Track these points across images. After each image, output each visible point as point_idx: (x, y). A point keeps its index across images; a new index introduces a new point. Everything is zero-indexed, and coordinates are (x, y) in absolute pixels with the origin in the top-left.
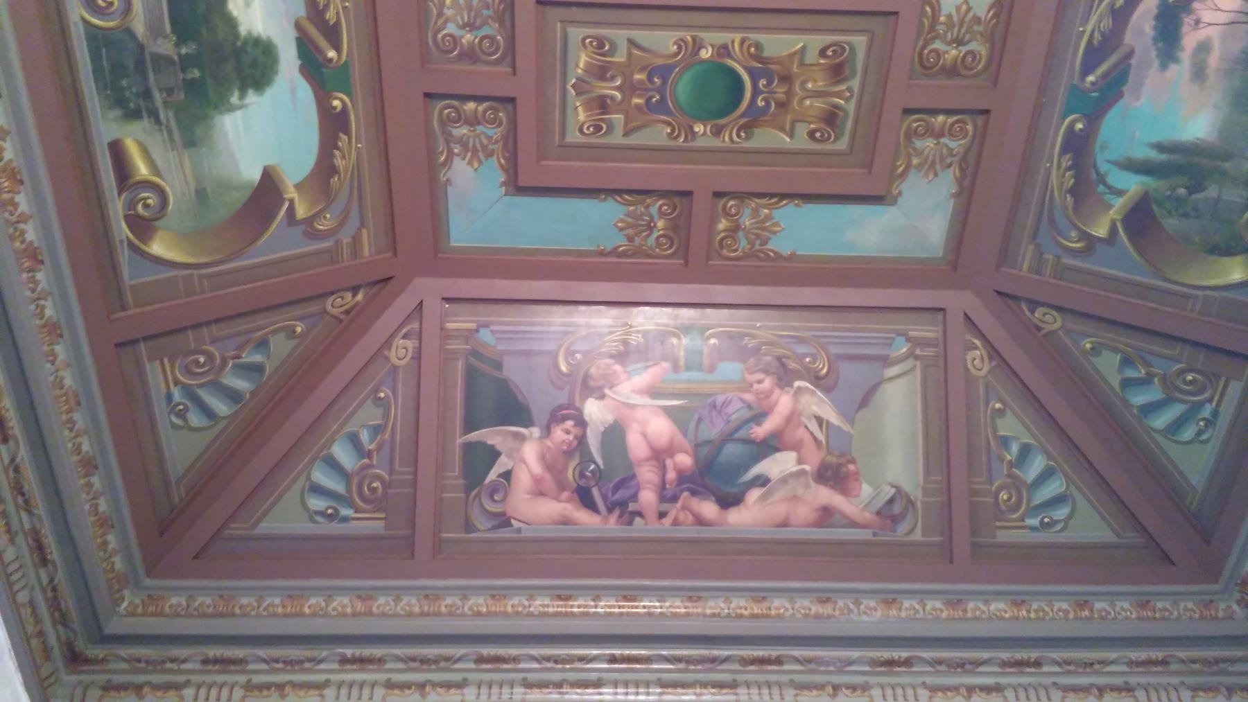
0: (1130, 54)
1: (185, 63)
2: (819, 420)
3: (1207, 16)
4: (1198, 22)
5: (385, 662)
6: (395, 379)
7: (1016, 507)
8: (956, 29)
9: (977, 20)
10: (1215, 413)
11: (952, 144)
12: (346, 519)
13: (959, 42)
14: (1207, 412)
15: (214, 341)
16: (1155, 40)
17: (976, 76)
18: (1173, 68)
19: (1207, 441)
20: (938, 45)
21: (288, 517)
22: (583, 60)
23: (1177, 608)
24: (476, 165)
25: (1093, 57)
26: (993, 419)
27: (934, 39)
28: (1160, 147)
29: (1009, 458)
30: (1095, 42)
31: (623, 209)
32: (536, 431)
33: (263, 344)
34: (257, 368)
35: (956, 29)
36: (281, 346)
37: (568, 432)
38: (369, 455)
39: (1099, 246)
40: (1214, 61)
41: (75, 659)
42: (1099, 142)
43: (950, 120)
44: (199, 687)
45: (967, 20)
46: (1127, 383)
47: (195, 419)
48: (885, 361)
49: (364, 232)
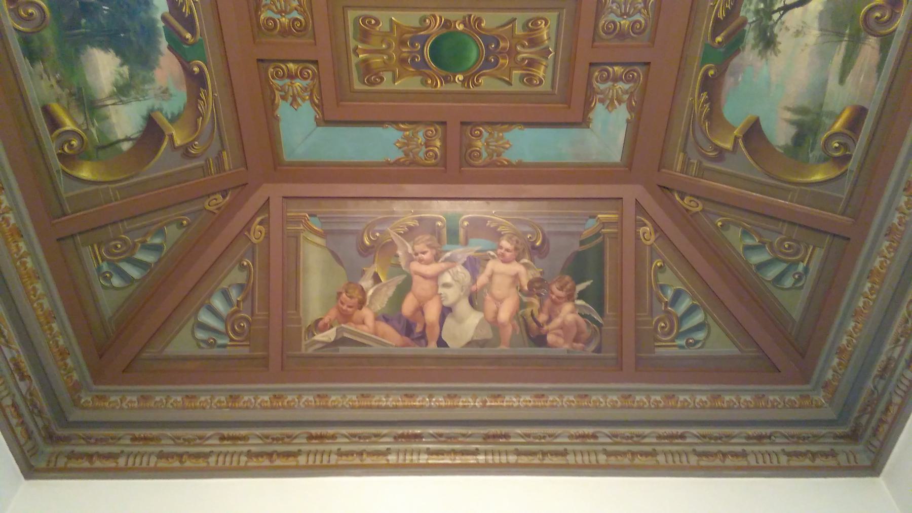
5: (248, 439)
6: (253, 252)
7: (669, 333)
10: (806, 270)
14: (801, 267)
15: (126, 233)
19: (802, 287)
21: (183, 343)
23: (780, 398)
26: (655, 276)
31: (400, 134)
33: (160, 232)
34: (157, 248)
36: (173, 232)
39: (727, 155)
41: (51, 438)
44: (128, 456)
46: (748, 248)
47: (116, 282)
49: (225, 153)
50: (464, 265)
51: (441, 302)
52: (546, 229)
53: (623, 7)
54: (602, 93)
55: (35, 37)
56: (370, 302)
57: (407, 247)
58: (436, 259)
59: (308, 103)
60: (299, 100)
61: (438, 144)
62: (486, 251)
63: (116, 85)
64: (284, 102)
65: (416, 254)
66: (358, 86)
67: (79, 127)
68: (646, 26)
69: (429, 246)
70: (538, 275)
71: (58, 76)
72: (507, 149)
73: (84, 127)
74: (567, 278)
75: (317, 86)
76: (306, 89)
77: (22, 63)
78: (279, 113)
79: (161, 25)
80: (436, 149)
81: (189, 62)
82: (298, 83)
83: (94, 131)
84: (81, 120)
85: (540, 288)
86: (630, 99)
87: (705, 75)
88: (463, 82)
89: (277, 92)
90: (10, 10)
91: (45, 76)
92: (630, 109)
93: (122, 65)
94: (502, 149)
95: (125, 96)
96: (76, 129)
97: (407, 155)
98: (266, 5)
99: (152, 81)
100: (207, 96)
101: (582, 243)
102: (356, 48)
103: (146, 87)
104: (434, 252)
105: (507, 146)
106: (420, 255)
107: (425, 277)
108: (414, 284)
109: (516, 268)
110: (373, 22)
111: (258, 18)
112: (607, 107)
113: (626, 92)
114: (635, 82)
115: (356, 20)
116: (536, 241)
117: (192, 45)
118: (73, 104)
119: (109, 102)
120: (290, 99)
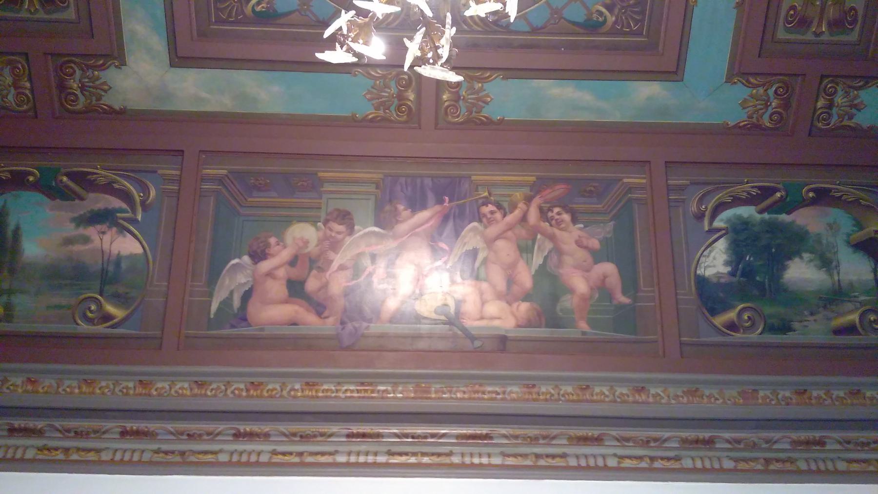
0: (82, 199)
3: (107, 238)
4: (104, 233)
8: (91, 84)
9: (99, 99)
11: (10, 97)
13: (83, 88)
16: (92, 211)
17: (62, 105)
18: (72, 226)
20: (78, 73)
24: (368, 96)
25: (79, 178)
27: (83, 70)
28: (17, 231)
30: (89, 177)
35: (91, 84)
40: (77, 248)
42: (19, 192)
43: (27, 92)
45: (99, 91)
55: (769, 321)
60: (856, 102)
63: (820, 268)
66: (854, 37)
67: (857, 309)
71: (806, 313)
73: (858, 305)
76: (846, 92)
77: (789, 338)
78: (865, 124)
79: (766, 216)
81: (804, 200)
82: (839, 99)
83: (862, 298)
84: (850, 306)
89: (843, 123)
90: (744, 333)
91: (806, 323)
93: (801, 258)
95: (831, 263)
96: (860, 311)
98: (757, 119)
99: (819, 235)
103: (824, 242)
110: (792, 12)
111: (767, 129)
115: (788, 30)
118: (834, 308)
119: (836, 278)
120: (854, 111)
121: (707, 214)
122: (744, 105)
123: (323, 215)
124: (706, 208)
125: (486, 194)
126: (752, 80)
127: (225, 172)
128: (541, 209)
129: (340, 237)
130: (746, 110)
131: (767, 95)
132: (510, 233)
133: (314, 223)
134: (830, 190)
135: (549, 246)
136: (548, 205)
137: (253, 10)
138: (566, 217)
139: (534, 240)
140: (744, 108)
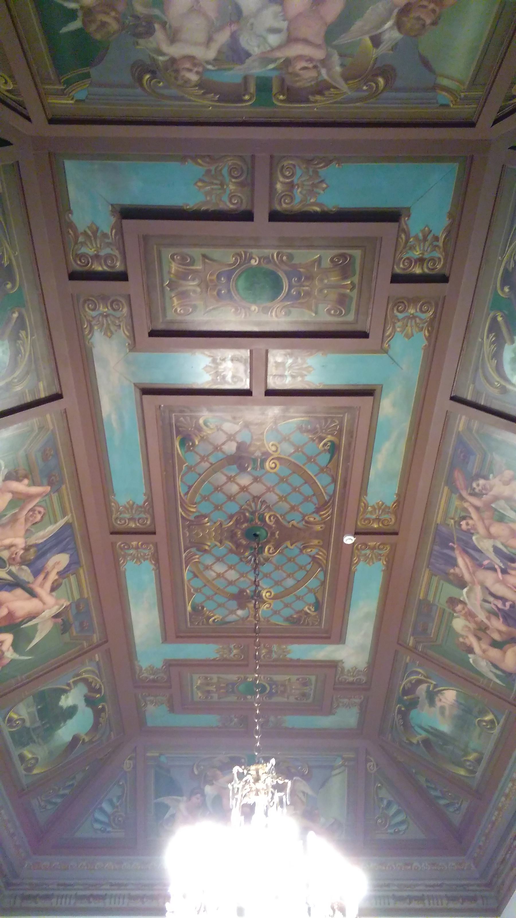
1: (43, 725)
2: (304, 793)
12: (108, 832)
22: (199, 682)
24: (109, 334)
29: (382, 806)
32: (185, 798)
37: (198, 799)
38: (117, 807)
48: (332, 768)
49: (112, 733)
50: (248, 55)
51: (284, 10)
52: (139, 90)
53: (109, 322)
54: (109, 245)
56: (391, 14)
57: (328, 74)
58: (288, 62)
59: (413, 233)
60: (421, 236)
61: (279, 186)
62: (219, 70)
64: (436, 235)
65: (315, 67)
68: (83, 307)
69: (297, 75)
70: (141, 41)
72: (201, 180)
74: (98, 37)
75: (398, 252)
80: (281, 179)
85: (136, 26)
86: (76, 237)
87: (13, 281)
88: (251, 258)
92: (71, 225)
94: (206, 179)
97: (316, 172)
100: (508, 262)
101: (87, 76)
102: (352, 290)
104: (290, 70)
105: (200, 184)
106: (311, 66)
107: (306, 41)
108: (323, 34)
109: (175, 51)
111: (435, 313)
112: (98, 229)
113: (83, 244)
114: (77, 255)
116: (151, 79)
117: (501, 310)
120: (430, 237)
121: (503, 383)
122: (409, 336)
123: (448, 610)
124: (498, 382)
125: (452, 521)
126: (388, 334)
127: (412, 638)
128: (471, 494)
129: (466, 610)
130: (415, 333)
131: (404, 318)
132: (487, 522)
133: (453, 617)
134: (506, 270)
135: (502, 503)
136: (469, 489)
137: (315, 611)
138: (482, 482)
139: (496, 510)
140: (413, 335)
